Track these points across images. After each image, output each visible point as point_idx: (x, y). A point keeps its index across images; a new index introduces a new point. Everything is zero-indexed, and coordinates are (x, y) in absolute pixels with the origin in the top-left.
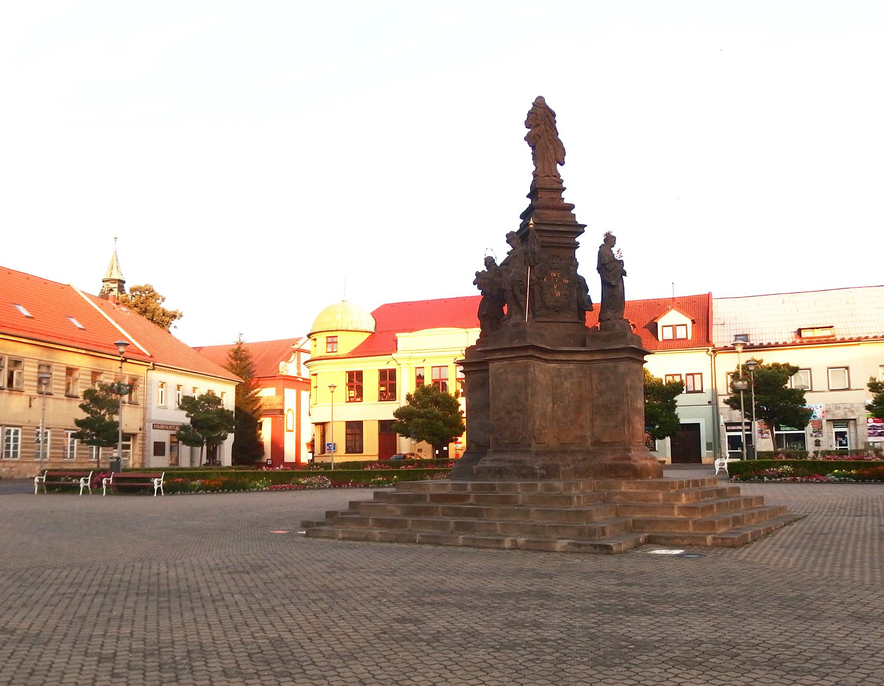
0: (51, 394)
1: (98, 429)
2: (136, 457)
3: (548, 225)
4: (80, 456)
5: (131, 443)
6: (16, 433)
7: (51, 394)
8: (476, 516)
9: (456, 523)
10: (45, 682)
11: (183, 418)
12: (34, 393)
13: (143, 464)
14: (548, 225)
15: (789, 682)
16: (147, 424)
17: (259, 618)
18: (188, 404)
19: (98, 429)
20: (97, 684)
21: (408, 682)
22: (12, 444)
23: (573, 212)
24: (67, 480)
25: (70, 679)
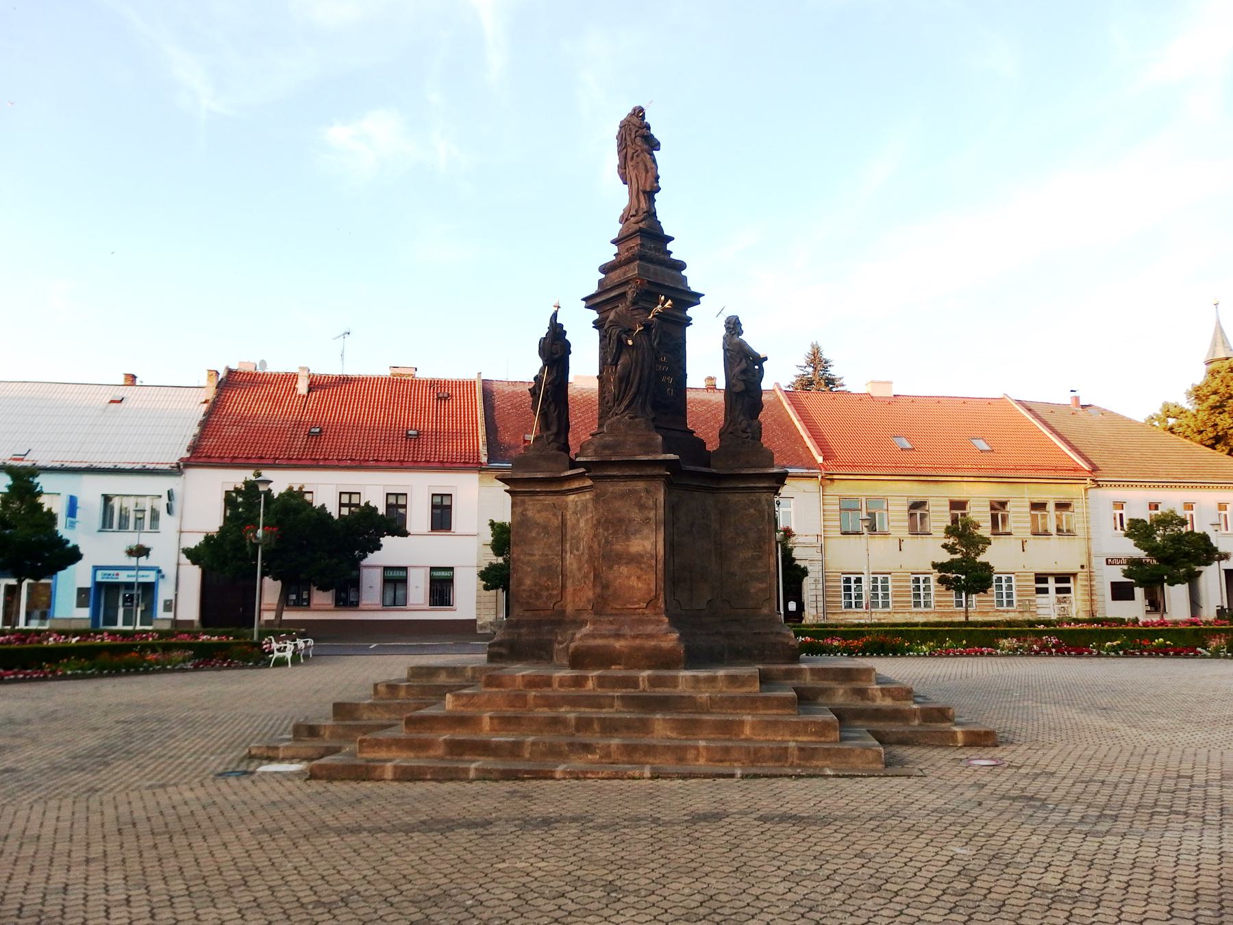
0: (1010, 534)
1: (967, 575)
2: (1079, 603)
3: (645, 290)
4: (941, 607)
5: (1071, 585)
6: (1009, 580)
7: (1010, 534)
8: (421, 668)
9: (599, 677)
10: (86, 920)
11: (1130, 549)
12: (904, 533)
13: (1092, 613)
14: (645, 290)
15: (910, 920)
16: (1094, 560)
17: (38, 822)
18: (1138, 531)
19: (967, 575)
20: (66, 923)
21: (521, 920)
22: (880, 593)
23: (683, 273)
24: (142, 639)
25: (1133, 910)
